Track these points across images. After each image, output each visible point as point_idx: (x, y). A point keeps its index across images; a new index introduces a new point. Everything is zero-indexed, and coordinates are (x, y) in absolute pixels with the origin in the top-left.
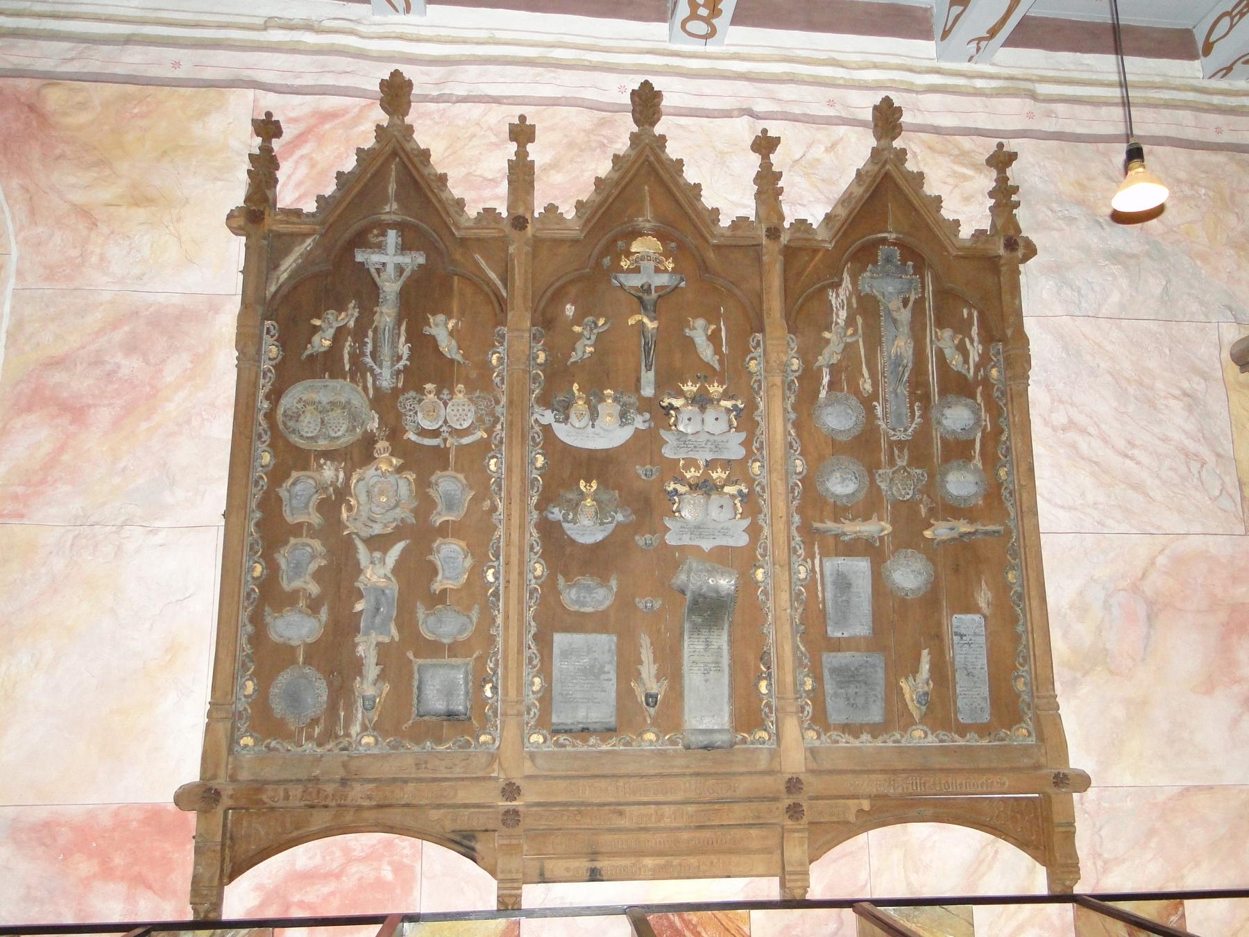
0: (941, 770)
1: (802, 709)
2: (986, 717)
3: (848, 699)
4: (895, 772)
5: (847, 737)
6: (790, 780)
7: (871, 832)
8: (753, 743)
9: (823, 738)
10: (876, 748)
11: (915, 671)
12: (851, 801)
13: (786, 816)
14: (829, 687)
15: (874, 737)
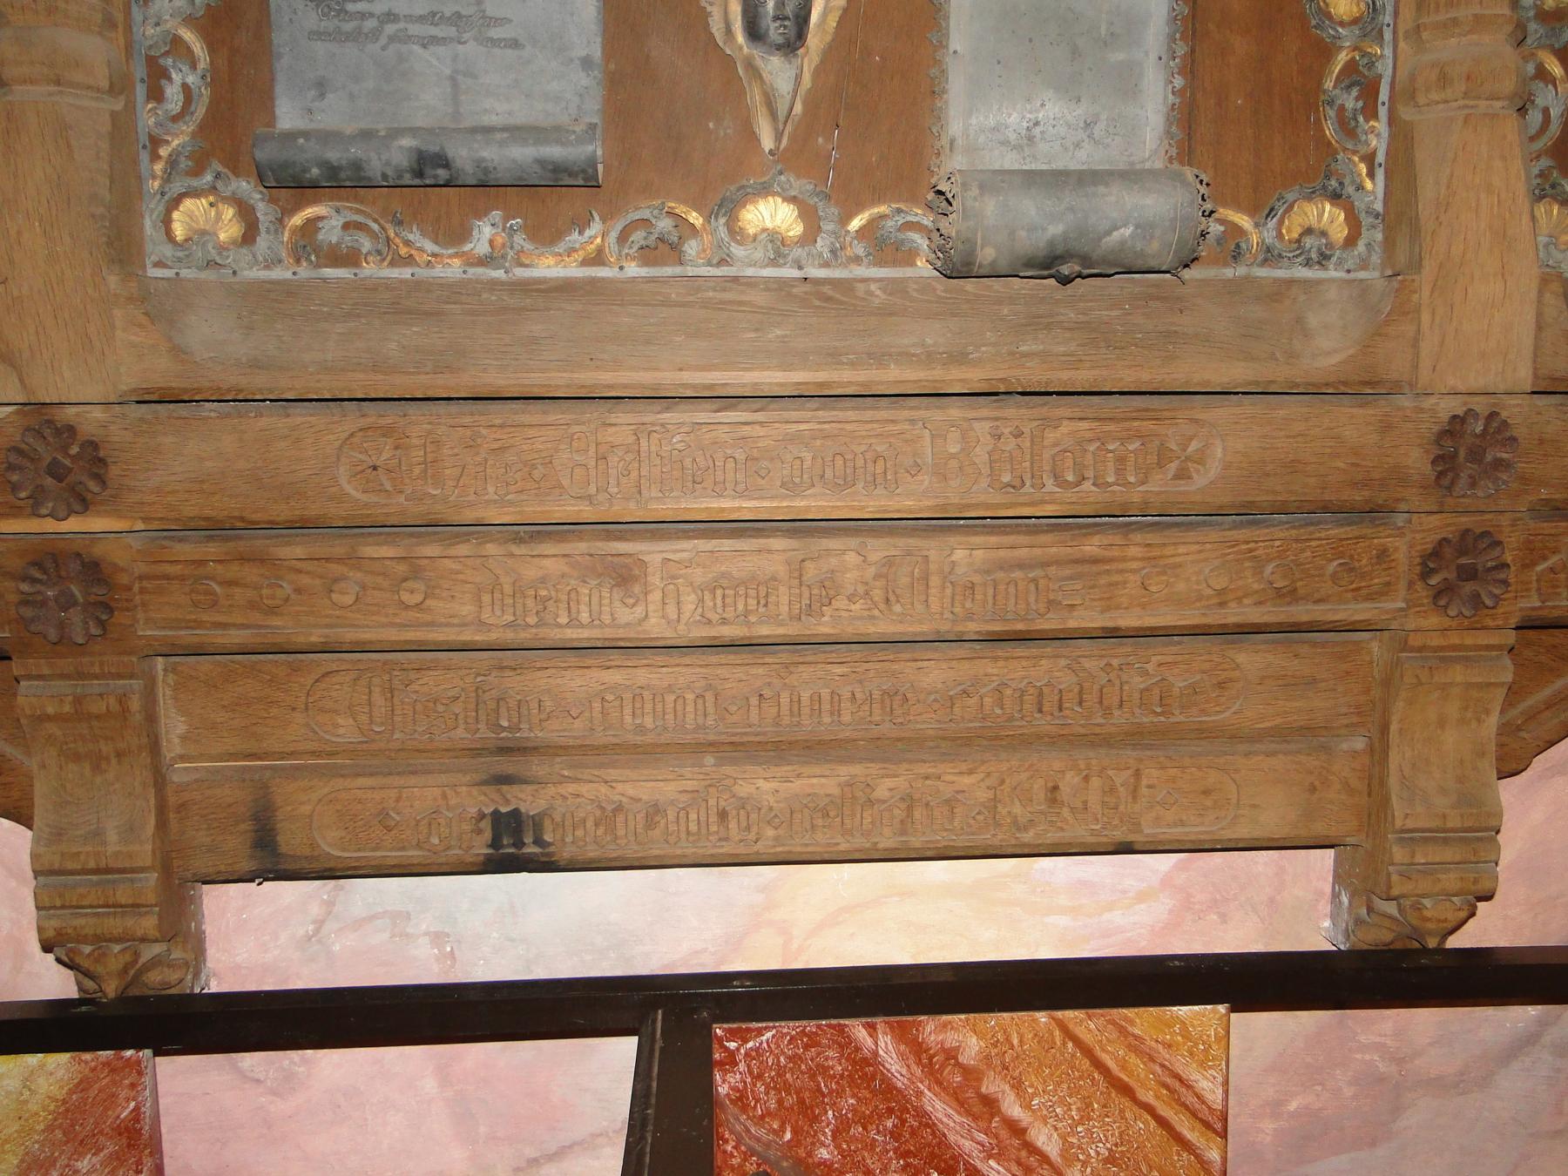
8: (1270, 256)
13: (1422, 593)
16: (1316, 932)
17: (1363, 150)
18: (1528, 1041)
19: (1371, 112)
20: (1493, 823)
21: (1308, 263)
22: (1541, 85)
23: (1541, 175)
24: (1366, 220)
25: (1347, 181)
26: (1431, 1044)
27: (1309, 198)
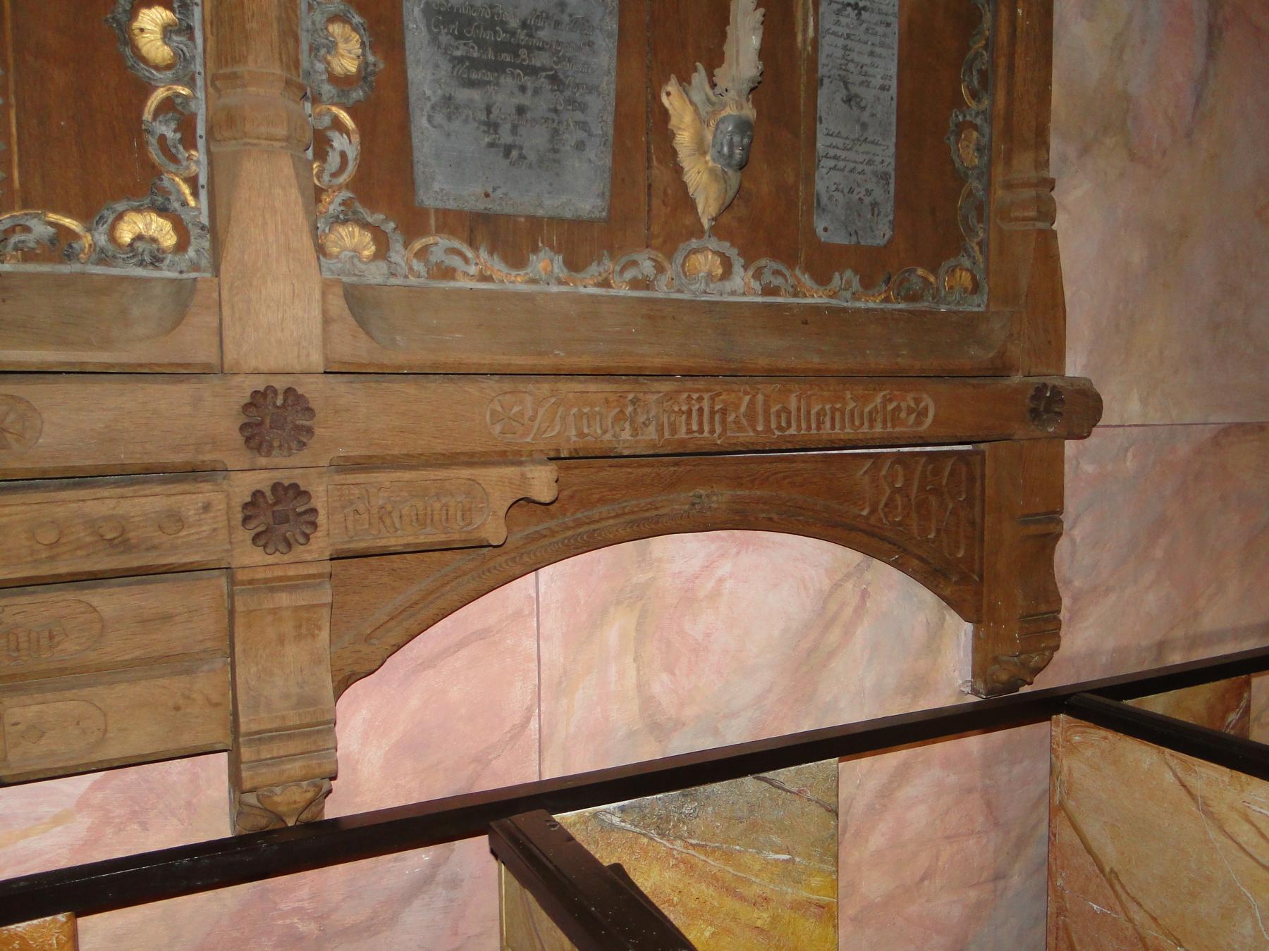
0: (771, 374)
1: (321, 144)
2: (882, 232)
3: (492, 126)
4: (637, 375)
5: (484, 259)
6: (258, 399)
7: (545, 573)
8: (103, 258)
9: (398, 254)
10: (579, 299)
11: (714, 60)
12: (494, 473)
13: (245, 535)
14: (425, 73)
15: (574, 265)
16: (214, 823)
17: (186, 174)
18: (426, 881)
19: (189, 141)
20: (328, 717)
21: (141, 264)
22: (337, 134)
23: (344, 203)
24: (194, 232)
25: (172, 198)
26: (343, 900)
27: (138, 210)
